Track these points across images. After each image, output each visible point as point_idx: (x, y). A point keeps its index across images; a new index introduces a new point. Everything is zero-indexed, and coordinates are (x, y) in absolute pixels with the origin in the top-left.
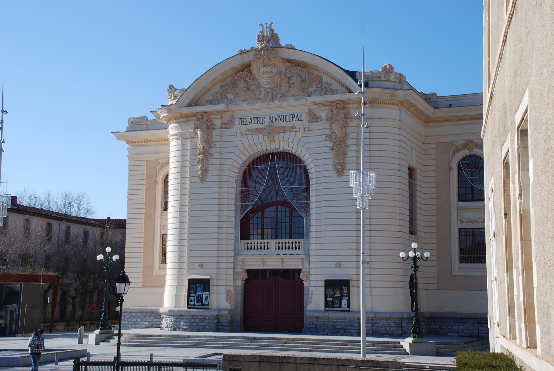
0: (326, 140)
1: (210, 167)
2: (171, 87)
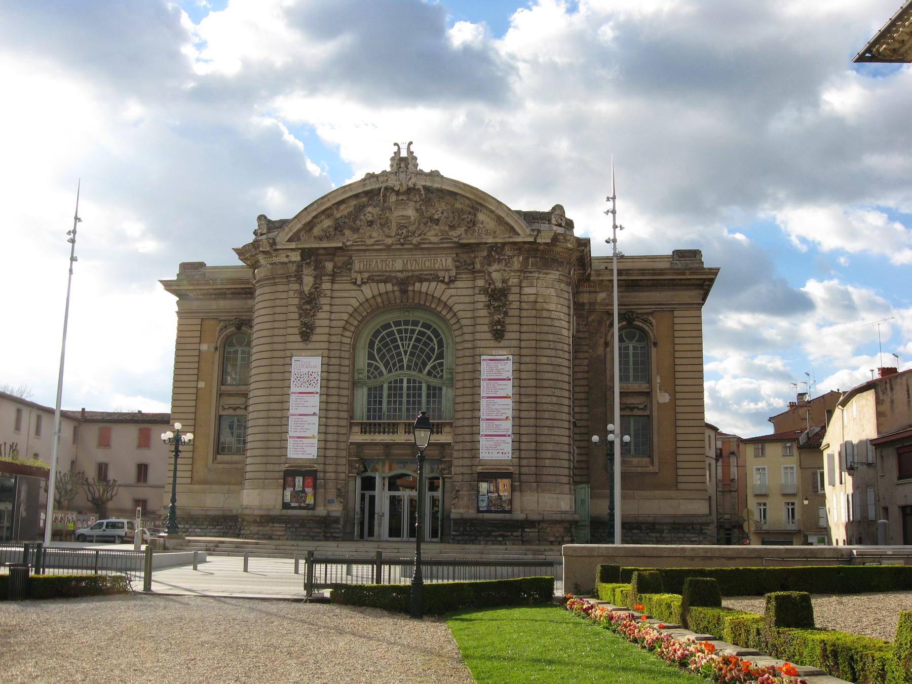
0: (480, 294)
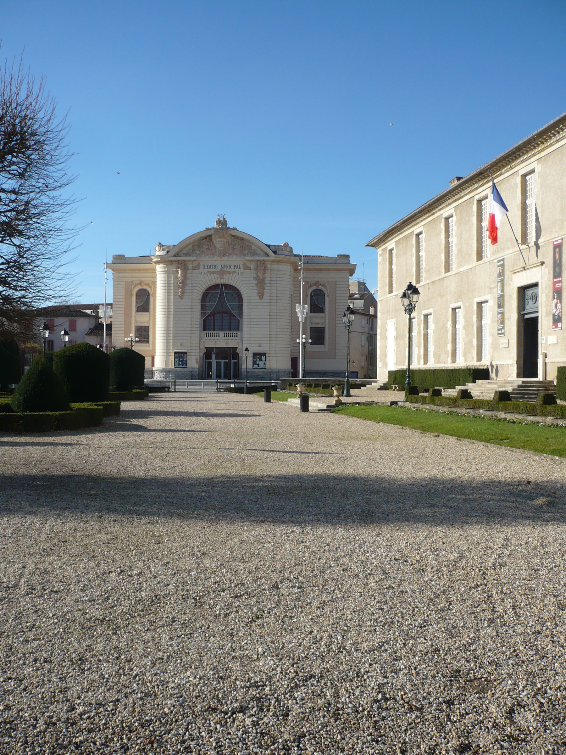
1: (186, 291)
2: (160, 244)
